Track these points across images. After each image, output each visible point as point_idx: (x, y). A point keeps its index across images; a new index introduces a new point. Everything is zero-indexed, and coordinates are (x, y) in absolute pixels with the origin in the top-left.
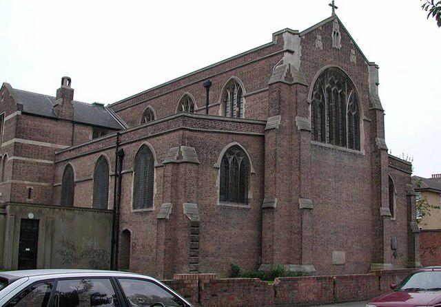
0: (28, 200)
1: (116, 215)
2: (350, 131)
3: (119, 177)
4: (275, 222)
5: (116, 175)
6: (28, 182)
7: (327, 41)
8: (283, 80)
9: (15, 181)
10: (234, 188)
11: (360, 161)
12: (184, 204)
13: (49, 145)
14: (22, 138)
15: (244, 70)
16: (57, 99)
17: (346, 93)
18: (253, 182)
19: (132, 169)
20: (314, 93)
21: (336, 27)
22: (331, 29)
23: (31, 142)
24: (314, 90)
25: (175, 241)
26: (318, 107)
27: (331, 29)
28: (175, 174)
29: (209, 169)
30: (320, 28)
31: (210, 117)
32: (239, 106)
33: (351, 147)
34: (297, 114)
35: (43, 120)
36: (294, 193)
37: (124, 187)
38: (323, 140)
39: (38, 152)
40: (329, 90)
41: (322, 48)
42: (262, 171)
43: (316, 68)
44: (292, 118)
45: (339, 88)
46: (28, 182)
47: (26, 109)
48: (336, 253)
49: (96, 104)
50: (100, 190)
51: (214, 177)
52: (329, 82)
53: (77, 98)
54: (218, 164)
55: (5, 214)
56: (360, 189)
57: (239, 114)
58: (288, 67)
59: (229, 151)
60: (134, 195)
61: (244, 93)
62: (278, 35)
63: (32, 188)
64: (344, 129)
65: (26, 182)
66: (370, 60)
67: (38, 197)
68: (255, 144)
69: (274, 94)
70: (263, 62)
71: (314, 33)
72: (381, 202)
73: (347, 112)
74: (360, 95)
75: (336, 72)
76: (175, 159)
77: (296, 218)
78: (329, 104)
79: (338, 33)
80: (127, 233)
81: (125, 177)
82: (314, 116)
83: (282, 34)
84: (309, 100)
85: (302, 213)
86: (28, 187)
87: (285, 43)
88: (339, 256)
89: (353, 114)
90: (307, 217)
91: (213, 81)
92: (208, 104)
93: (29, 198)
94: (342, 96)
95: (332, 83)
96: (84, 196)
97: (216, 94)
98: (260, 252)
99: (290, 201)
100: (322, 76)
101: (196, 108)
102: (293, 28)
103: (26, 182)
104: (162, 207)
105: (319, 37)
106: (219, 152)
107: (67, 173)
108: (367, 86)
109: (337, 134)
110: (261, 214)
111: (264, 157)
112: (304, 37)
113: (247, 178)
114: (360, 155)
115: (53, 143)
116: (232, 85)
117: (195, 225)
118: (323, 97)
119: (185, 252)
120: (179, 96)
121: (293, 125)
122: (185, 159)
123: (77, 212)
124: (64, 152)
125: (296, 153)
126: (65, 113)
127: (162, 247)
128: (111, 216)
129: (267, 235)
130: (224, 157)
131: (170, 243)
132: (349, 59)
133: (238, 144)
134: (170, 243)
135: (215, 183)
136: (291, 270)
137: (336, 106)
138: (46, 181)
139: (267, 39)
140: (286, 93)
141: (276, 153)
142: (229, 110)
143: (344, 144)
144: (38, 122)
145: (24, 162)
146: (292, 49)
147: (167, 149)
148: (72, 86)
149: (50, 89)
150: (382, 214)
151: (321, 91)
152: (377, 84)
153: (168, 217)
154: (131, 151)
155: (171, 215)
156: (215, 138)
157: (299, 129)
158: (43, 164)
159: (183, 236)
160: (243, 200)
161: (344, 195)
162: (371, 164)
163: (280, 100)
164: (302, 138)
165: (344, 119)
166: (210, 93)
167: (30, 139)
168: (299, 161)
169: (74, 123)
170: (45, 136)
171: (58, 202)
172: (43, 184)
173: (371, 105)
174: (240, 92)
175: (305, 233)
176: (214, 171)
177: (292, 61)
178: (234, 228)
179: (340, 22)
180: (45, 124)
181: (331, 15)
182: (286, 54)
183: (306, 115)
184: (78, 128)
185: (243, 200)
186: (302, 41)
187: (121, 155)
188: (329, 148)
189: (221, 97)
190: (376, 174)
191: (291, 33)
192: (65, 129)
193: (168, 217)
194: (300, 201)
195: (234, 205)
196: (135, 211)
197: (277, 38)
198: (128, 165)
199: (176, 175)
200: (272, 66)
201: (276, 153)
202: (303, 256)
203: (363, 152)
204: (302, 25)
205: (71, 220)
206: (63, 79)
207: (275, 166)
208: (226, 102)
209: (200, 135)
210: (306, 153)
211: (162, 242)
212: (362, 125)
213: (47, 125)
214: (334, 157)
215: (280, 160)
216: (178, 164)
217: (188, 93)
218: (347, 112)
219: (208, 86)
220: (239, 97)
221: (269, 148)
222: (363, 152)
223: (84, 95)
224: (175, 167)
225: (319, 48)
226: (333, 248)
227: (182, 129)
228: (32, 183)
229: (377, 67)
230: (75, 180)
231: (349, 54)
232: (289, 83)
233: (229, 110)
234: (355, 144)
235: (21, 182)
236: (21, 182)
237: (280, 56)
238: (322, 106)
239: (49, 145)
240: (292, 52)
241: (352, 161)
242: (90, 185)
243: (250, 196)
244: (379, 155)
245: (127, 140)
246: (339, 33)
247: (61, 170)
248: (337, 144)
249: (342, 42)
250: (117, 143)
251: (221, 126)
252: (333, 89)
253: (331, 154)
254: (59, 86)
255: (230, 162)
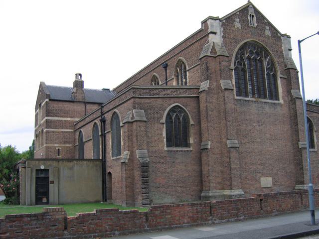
0: (58, 156)
1: (103, 162)
2: (269, 87)
3: (104, 135)
4: (210, 159)
5: (102, 135)
6: (58, 145)
7: (244, 22)
8: (209, 54)
9: (48, 145)
10: (178, 135)
11: (279, 108)
12: (137, 151)
13: (69, 119)
14: (51, 116)
15: (186, 52)
16: (74, 90)
17: (263, 59)
18: (192, 131)
19: (91, 138)
20: (236, 62)
21: (251, 11)
22: (247, 13)
23: (57, 118)
24: (268, 65)
25: (133, 177)
26: (240, 71)
27: (247, 13)
28: (130, 131)
29: (156, 125)
30: (238, 13)
31: (168, 87)
32: (186, 78)
33: (271, 98)
34: (221, 77)
35: (64, 103)
36: (223, 136)
37: (107, 143)
38: (247, 95)
39: (63, 125)
40: (249, 58)
41: (240, 28)
42: (199, 123)
43: (237, 42)
44: (217, 81)
45: (258, 55)
46: (58, 145)
47: (52, 98)
48: (263, 179)
49: (103, 89)
50: (96, 146)
51: (161, 130)
52: (252, 54)
53: (86, 86)
54: (164, 120)
55: (25, 167)
56: (283, 129)
57: (186, 83)
58: (212, 45)
59: (173, 110)
60: (112, 147)
61: (188, 68)
62: (204, 22)
63: (60, 148)
64: (264, 86)
65: (56, 145)
66: (282, 33)
67: (65, 154)
68: (193, 104)
69: (204, 65)
70: (197, 44)
71: (233, 17)
72: (299, 138)
73: (266, 73)
74: (276, 60)
75: (254, 44)
76: (130, 120)
77: (226, 155)
78: (249, 68)
79: (253, 16)
80: (110, 173)
81: (107, 135)
82: (238, 79)
83: (207, 21)
84: (232, 66)
85: (230, 151)
86: (57, 148)
87: (209, 27)
88: (266, 182)
89: (271, 74)
90: (234, 153)
91: (169, 63)
92: (166, 79)
93: (59, 155)
94: (261, 61)
95: (251, 52)
96: (89, 153)
97: (171, 71)
98: (201, 182)
99: (221, 143)
100: (242, 48)
101: (160, 83)
102: (215, 16)
103: (56, 145)
104: (125, 154)
105: (237, 20)
106: (164, 112)
107: (80, 137)
108: (282, 53)
109: (259, 90)
110: (201, 153)
111: (200, 112)
112: (224, 21)
113: (188, 129)
114: (280, 104)
115: (72, 117)
116: (180, 64)
117: (145, 167)
118: (244, 64)
119: (139, 185)
120: (149, 77)
121: (219, 86)
122: (136, 118)
123: (75, 162)
124: (78, 122)
125: (223, 107)
126: (79, 97)
127: (124, 183)
128: (100, 164)
129: (205, 169)
130: (168, 114)
131: (129, 180)
132: (264, 33)
133: (179, 105)
134: (129, 180)
135: (162, 134)
136: (225, 193)
137: (256, 70)
138: (69, 143)
139: (199, 27)
140: (213, 65)
141: (207, 108)
142: (180, 80)
143: (265, 97)
144: (60, 105)
145: (53, 132)
146: (215, 31)
147: (127, 113)
148: (83, 79)
149: (69, 83)
150: (300, 147)
151: (242, 59)
152: (290, 50)
153: (127, 161)
154: (108, 117)
155: (129, 159)
156: (160, 102)
157: (223, 88)
158: (67, 132)
159: (137, 173)
160: (187, 145)
161: (268, 136)
162: (290, 110)
163: (207, 69)
164: (226, 95)
165: (263, 78)
166: (167, 71)
167: (56, 116)
168: (225, 113)
169: (86, 103)
170: (66, 114)
171: (77, 157)
172: (67, 145)
173: (286, 66)
174: (185, 68)
175: (233, 166)
176: (161, 126)
177: (216, 39)
178: (180, 166)
179: (254, 7)
180: (66, 106)
181: (247, 3)
182: (211, 35)
183: (230, 78)
184: (88, 106)
185: (187, 145)
186: (223, 25)
187: (103, 121)
188: (252, 101)
189: (174, 73)
190: (294, 118)
191: (213, 19)
192: (80, 108)
193: (127, 161)
194: (228, 142)
195: (180, 149)
196: (113, 158)
197: (204, 25)
198: (108, 126)
199: (132, 131)
200: (202, 45)
201: (207, 108)
202: (233, 183)
203: (281, 101)
204: (222, 12)
205: (71, 168)
206: (76, 75)
207: (207, 118)
208: (178, 76)
209: (147, 101)
210: (230, 105)
211: (124, 180)
212: (279, 81)
213: (67, 106)
214: (256, 109)
215: (210, 113)
216: (132, 122)
217: (155, 74)
218: (266, 73)
219: (166, 67)
220: (185, 72)
221: (203, 105)
222: (281, 101)
223: (92, 84)
224: (130, 125)
225: (238, 28)
226: (261, 175)
227: (133, 97)
228: (60, 145)
229: (289, 37)
230: (84, 140)
231: (263, 30)
232: (214, 56)
233: (180, 80)
234: (274, 95)
235: (52, 145)
236: (52, 145)
237: (206, 38)
238: (244, 70)
239: (69, 119)
240: (215, 33)
241: (273, 109)
242: (91, 143)
243: (191, 141)
244: (294, 103)
245: (107, 110)
246: (255, 15)
247: (78, 133)
248: (259, 97)
249: (257, 22)
250: (102, 113)
251: (164, 93)
252: (252, 57)
253: (254, 105)
254: (74, 79)
255: (173, 118)
